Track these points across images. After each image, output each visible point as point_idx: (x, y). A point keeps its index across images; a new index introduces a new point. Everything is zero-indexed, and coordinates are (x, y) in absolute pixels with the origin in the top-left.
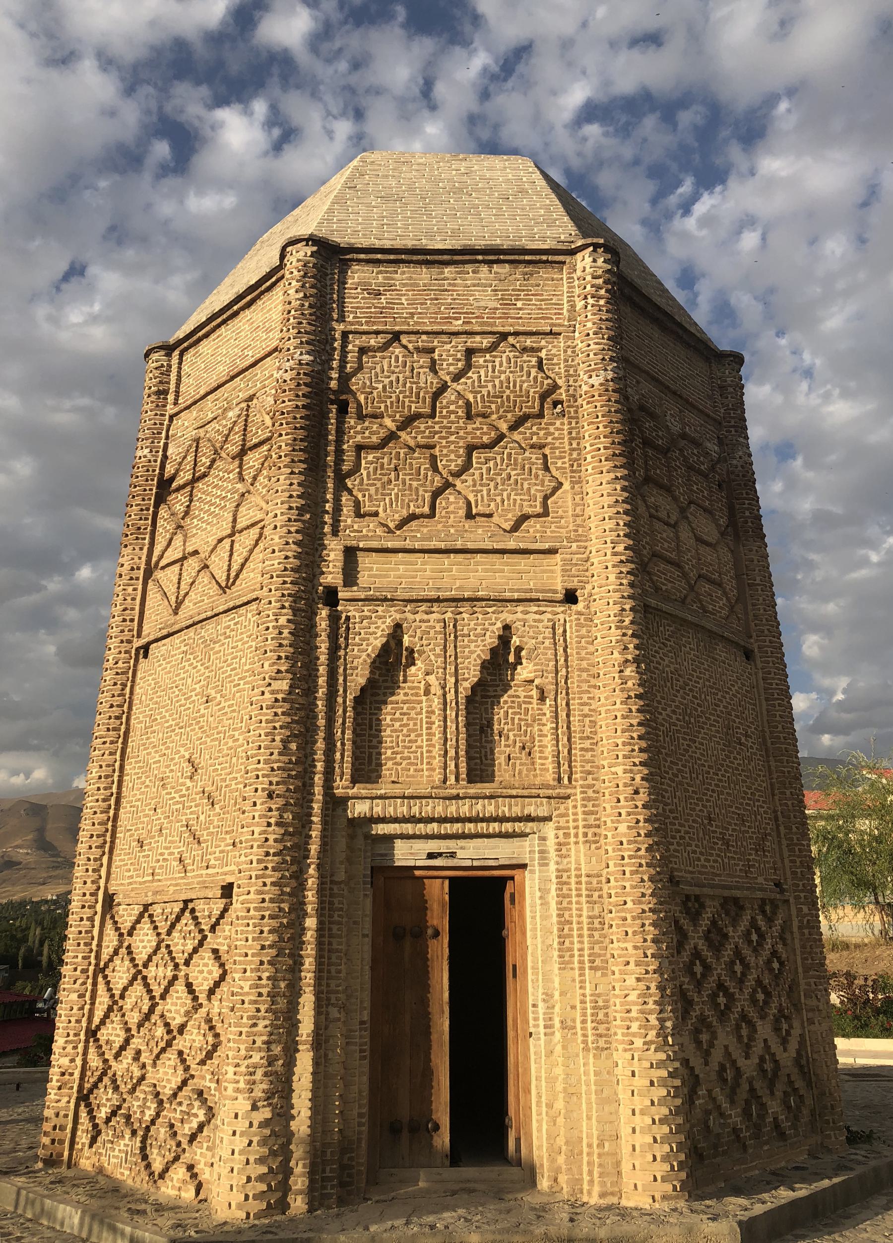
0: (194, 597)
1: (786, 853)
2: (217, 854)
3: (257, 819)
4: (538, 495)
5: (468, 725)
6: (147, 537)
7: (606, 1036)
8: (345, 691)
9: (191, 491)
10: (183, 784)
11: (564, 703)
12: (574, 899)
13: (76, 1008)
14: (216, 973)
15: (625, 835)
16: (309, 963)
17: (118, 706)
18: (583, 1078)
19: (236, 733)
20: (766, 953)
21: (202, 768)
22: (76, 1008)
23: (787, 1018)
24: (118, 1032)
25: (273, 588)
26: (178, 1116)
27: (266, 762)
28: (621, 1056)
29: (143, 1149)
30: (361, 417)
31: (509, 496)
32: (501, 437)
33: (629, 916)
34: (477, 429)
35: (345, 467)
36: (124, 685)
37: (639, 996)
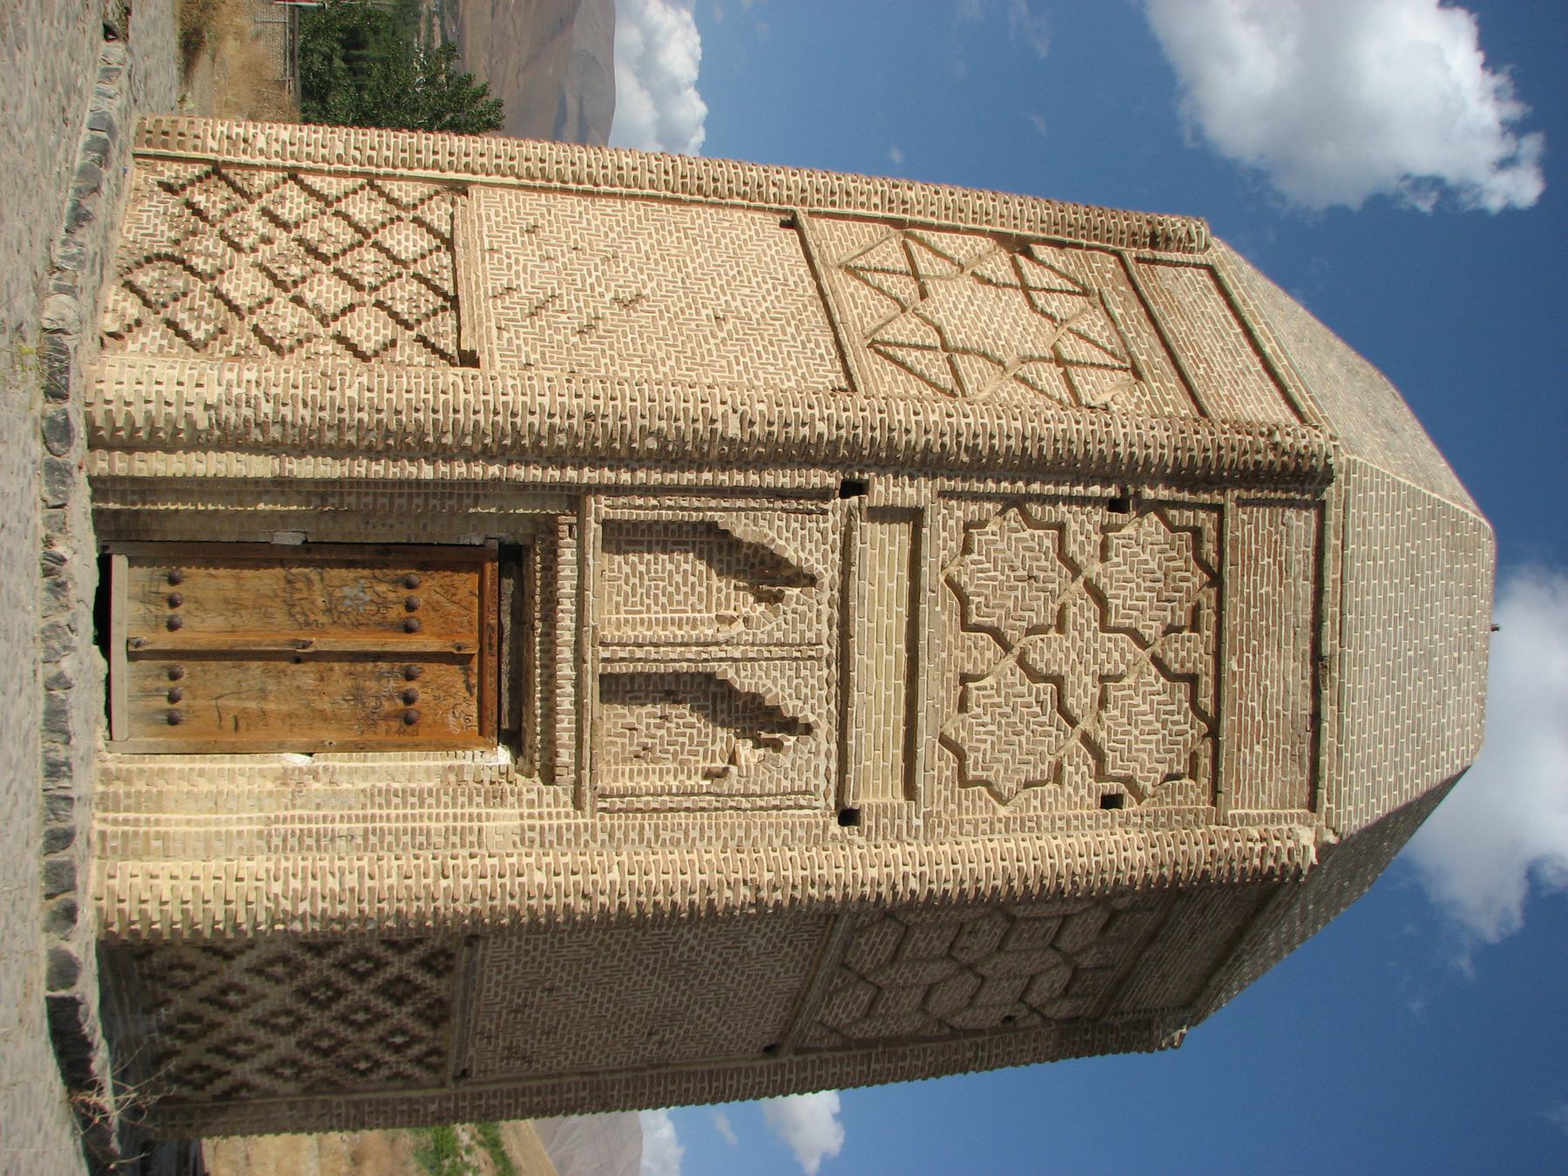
0: (862, 293)
1: (505, 1087)
2: (515, 342)
3: (559, 399)
4: (992, 774)
5: (677, 675)
8: (725, 509)
9: (1011, 286)
10: (608, 289)
11: (704, 805)
12: (450, 811)
13: (326, 151)
15: (531, 880)
16: (379, 469)
17: (716, 189)
18: (235, 816)
19: (673, 363)
20: (379, 1053)
21: (629, 315)
22: (326, 151)
23: (297, 1076)
24: (295, 212)
25: (867, 413)
26: (198, 303)
28: (260, 864)
29: (159, 257)
30: (1104, 529)
31: (992, 733)
32: (1073, 722)
33: (429, 881)
35: (1035, 509)
36: (744, 196)
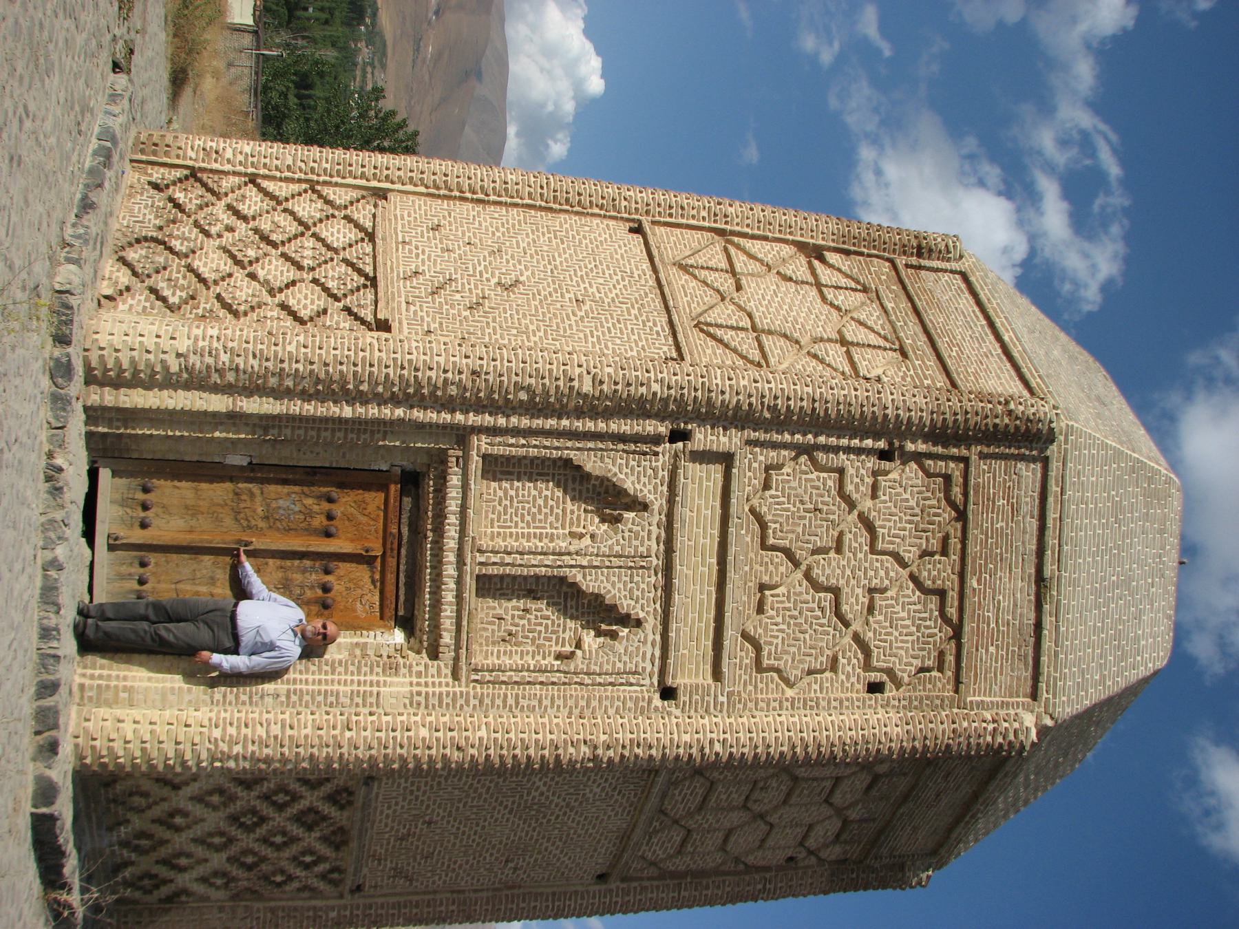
0: (691, 285)
1: (392, 900)
2: (420, 313)
4: (782, 663)
5: (537, 577)
6: (761, 233)
7: (224, 702)
8: (579, 449)
9: (807, 283)
10: (493, 275)
12: (356, 678)
13: (278, 163)
14: (304, 314)
15: (417, 734)
19: (542, 334)
22: (278, 163)
23: (227, 884)
24: (253, 208)
25: (691, 378)
26: (174, 275)
27: (509, 369)
29: (146, 239)
30: (875, 474)
31: (782, 631)
32: (847, 624)
33: (337, 732)
34: (857, 600)
35: (821, 456)
37: (260, 737)
